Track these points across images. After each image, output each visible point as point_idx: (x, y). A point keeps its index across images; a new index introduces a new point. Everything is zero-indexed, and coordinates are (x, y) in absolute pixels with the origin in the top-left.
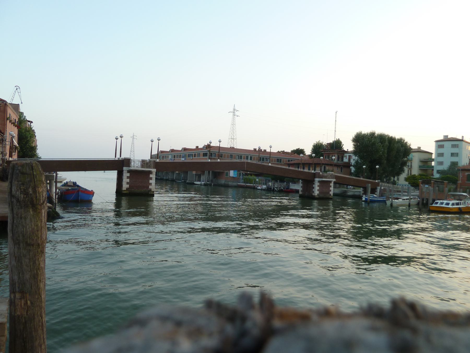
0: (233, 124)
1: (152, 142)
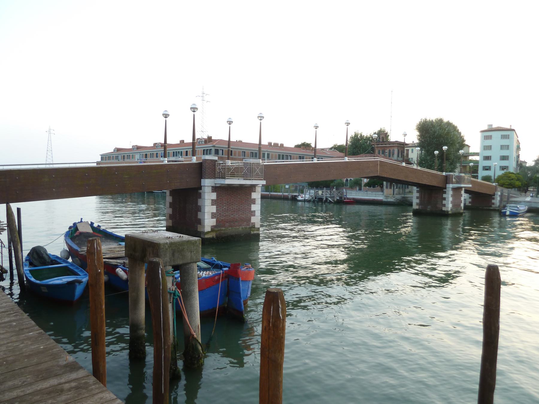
1: (230, 124)
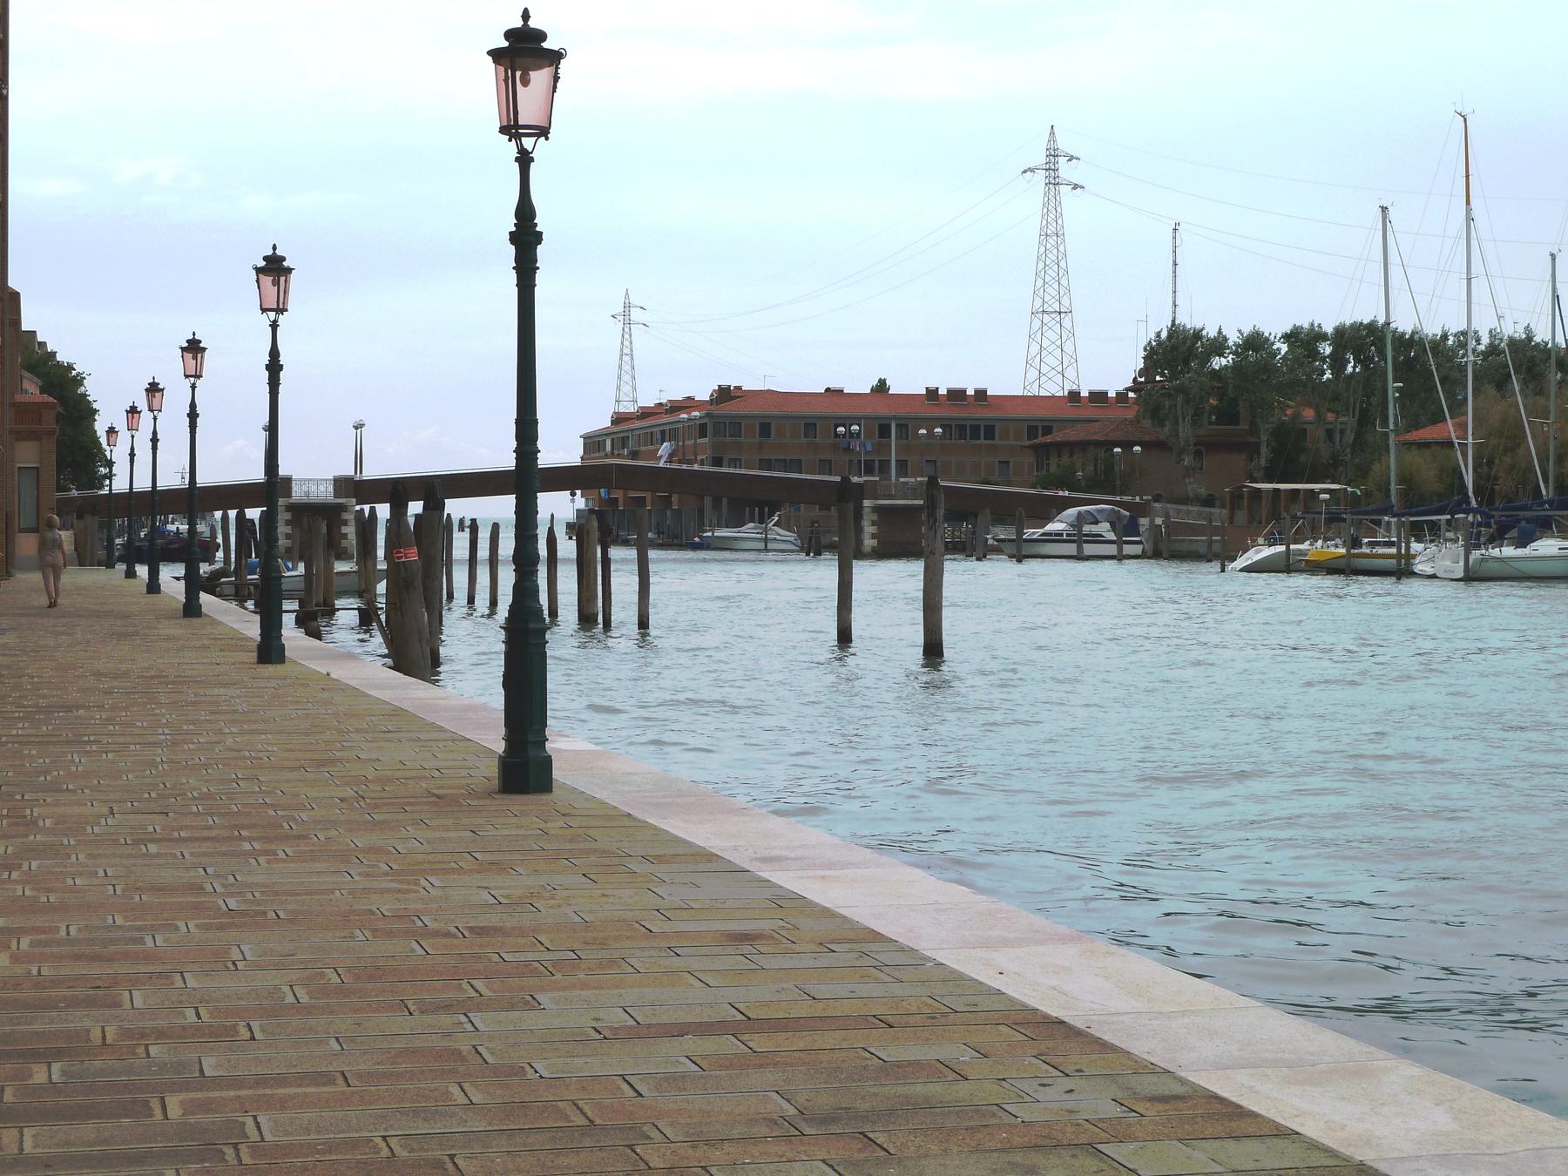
0: (1052, 232)
